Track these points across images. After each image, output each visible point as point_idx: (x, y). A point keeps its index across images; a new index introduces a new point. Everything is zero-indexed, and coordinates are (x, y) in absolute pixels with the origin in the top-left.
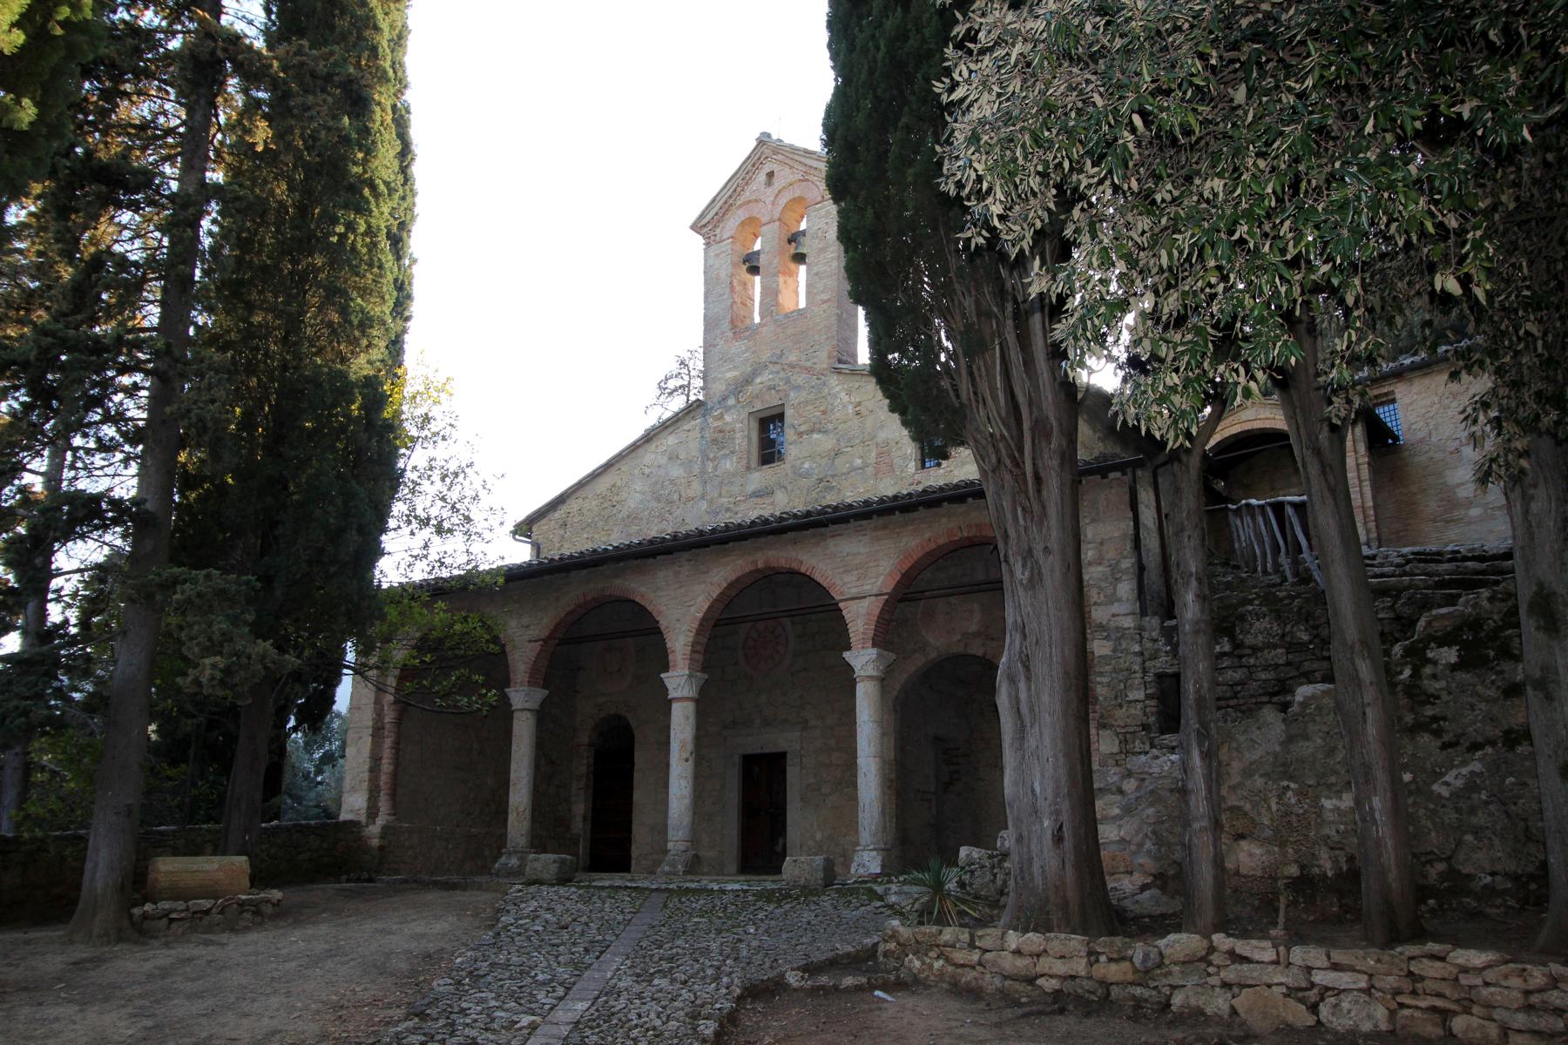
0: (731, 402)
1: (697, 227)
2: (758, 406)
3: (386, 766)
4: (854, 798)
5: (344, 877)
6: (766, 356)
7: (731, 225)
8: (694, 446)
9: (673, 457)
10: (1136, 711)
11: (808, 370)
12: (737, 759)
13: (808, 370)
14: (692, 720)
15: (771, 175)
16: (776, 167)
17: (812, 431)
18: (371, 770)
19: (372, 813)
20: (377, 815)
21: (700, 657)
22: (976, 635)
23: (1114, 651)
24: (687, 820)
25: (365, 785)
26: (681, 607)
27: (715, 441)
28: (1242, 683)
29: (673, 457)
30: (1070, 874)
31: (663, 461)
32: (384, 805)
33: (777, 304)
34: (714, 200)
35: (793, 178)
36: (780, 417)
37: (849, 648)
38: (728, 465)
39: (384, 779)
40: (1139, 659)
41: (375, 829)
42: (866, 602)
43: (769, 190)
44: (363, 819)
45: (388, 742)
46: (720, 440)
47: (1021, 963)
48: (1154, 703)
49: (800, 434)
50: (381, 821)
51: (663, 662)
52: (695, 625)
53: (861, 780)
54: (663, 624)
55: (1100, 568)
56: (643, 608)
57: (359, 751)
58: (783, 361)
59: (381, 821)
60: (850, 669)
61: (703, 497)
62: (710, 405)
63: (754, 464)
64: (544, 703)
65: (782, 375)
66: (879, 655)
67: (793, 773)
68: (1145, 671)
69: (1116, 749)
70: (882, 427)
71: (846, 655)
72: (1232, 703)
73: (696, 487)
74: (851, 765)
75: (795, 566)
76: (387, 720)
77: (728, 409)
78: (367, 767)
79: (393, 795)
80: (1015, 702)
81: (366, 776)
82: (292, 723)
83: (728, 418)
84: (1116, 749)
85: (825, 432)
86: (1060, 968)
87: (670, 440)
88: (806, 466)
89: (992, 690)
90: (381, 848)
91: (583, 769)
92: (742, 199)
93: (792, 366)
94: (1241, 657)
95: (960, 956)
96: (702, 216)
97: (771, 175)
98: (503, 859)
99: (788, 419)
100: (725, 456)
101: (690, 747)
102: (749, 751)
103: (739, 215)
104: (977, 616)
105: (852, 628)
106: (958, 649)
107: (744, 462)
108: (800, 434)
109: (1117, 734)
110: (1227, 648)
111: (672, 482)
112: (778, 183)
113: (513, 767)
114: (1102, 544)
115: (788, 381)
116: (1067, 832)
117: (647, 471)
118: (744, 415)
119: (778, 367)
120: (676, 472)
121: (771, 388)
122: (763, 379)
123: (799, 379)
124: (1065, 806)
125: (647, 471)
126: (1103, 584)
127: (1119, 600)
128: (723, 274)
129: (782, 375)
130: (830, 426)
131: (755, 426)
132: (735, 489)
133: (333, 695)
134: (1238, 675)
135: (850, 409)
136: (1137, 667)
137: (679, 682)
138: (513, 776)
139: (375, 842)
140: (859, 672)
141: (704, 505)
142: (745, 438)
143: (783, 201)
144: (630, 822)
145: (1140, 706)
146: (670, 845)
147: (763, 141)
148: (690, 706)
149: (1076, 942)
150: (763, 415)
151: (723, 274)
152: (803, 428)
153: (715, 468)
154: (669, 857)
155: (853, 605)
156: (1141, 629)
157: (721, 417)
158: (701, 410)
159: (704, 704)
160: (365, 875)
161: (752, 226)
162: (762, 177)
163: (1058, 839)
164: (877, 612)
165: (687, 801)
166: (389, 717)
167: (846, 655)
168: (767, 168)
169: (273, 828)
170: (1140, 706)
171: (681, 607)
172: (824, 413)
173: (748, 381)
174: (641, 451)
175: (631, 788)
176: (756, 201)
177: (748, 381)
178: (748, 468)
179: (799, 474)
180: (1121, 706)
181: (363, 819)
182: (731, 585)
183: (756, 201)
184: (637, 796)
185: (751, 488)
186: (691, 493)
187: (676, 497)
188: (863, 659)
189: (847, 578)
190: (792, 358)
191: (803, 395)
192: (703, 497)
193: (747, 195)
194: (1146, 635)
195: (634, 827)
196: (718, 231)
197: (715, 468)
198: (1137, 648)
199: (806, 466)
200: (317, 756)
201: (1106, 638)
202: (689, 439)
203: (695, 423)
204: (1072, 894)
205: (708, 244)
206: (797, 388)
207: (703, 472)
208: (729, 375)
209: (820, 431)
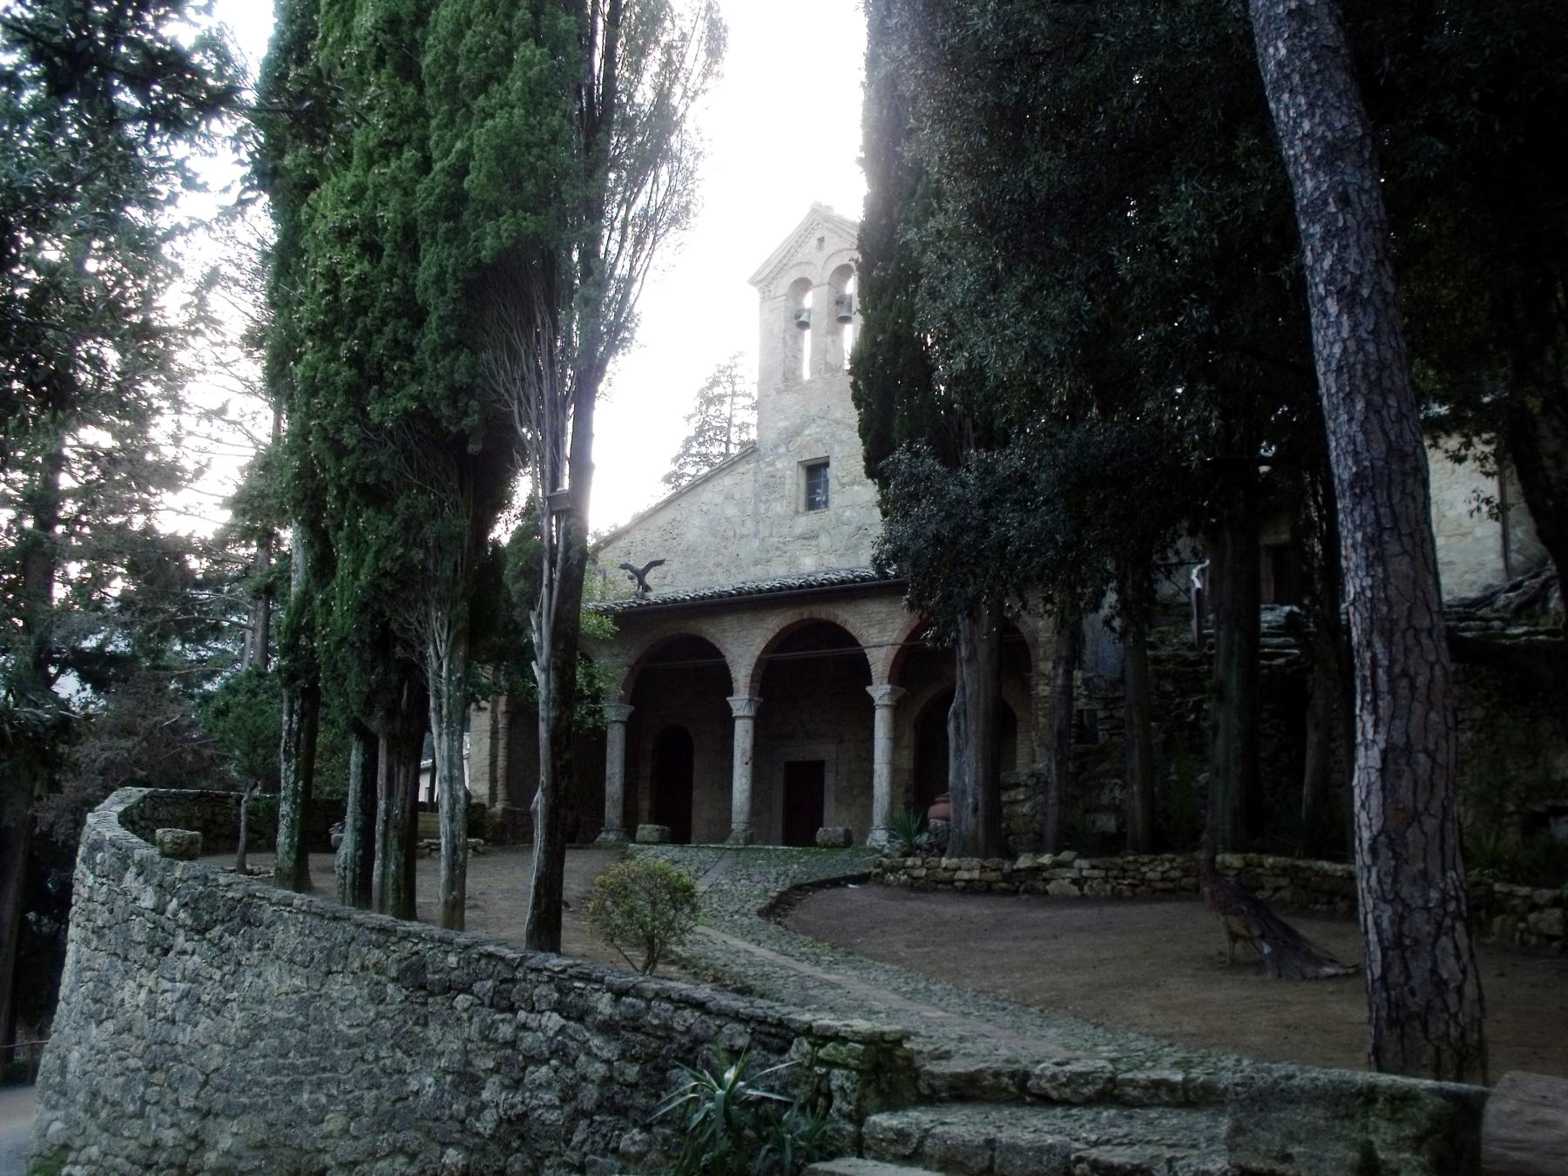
0: (782, 450)
1: (754, 282)
2: (806, 457)
4: (871, 796)
6: (814, 410)
8: (748, 488)
15: (821, 240)
16: (826, 234)
19: (493, 796)
21: (757, 686)
24: (746, 808)
26: (743, 650)
27: (766, 485)
29: (729, 497)
30: (981, 828)
31: (720, 499)
35: (841, 246)
36: (827, 465)
37: (870, 683)
38: (779, 508)
39: (500, 772)
42: (884, 650)
45: (502, 743)
46: (771, 485)
47: (947, 875)
49: (843, 485)
52: (754, 660)
53: (876, 780)
56: (713, 646)
59: (499, 806)
60: (871, 700)
61: (756, 535)
63: (801, 508)
64: (630, 717)
65: (828, 429)
66: (892, 690)
67: (830, 779)
71: (868, 689)
73: (750, 526)
74: (870, 773)
75: (832, 618)
77: (780, 456)
79: (508, 786)
80: (957, 729)
83: (779, 465)
86: (966, 876)
87: (727, 481)
88: (848, 514)
89: (945, 723)
91: (649, 771)
95: (916, 873)
97: (821, 240)
98: (603, 835)
100: (776, 499)
101: (749, 754)
103: (795, 275)
105: (873, 669)
107: (792, 507)
108: (843, 485)
111: (727, 519)
113: (608, 765)
115: (833, 436)
116: (980, 805)
118: (794, 463)
119: (825, 422)
120: (731, 510)
121: (817, 441)
122: (812, 431)
124: (980, 791)
129: (828, 429)
131: (802, 474)
132: (785, 531)
137: (740, 703)
138: (608, 772)
140: (877, 702)
141: (756, 543)
142: (794, 483)
146: (734, 826)
149: (975, 861)
152: (845, 480)
154: (733, 834)
157: (772, 464)
158: (755, 456)
159: (761, 722)
162: (814, 242)
163: (975, 810)
164: (892, 657)
165: (747, 794)
167: (868, 689)
168: (818, 234)
171: (743, 650)
173: (798, 432)
174: (700, 489)
178: (797, 512)
179: (841, 522)
182: (782, 631)
185: (798, 530)
186: (745, 531)
187: (731, 534)
188: (880, 691)
189: (871, 631)
192: (756, 535)
197: (767, 510)
199: (848, 514)
202: (742, 482)
203: (748, 467)
204: (981, 840)
205: (763, 299)
206: (841, 442)
207: (756, 513)
208: (781, 424)
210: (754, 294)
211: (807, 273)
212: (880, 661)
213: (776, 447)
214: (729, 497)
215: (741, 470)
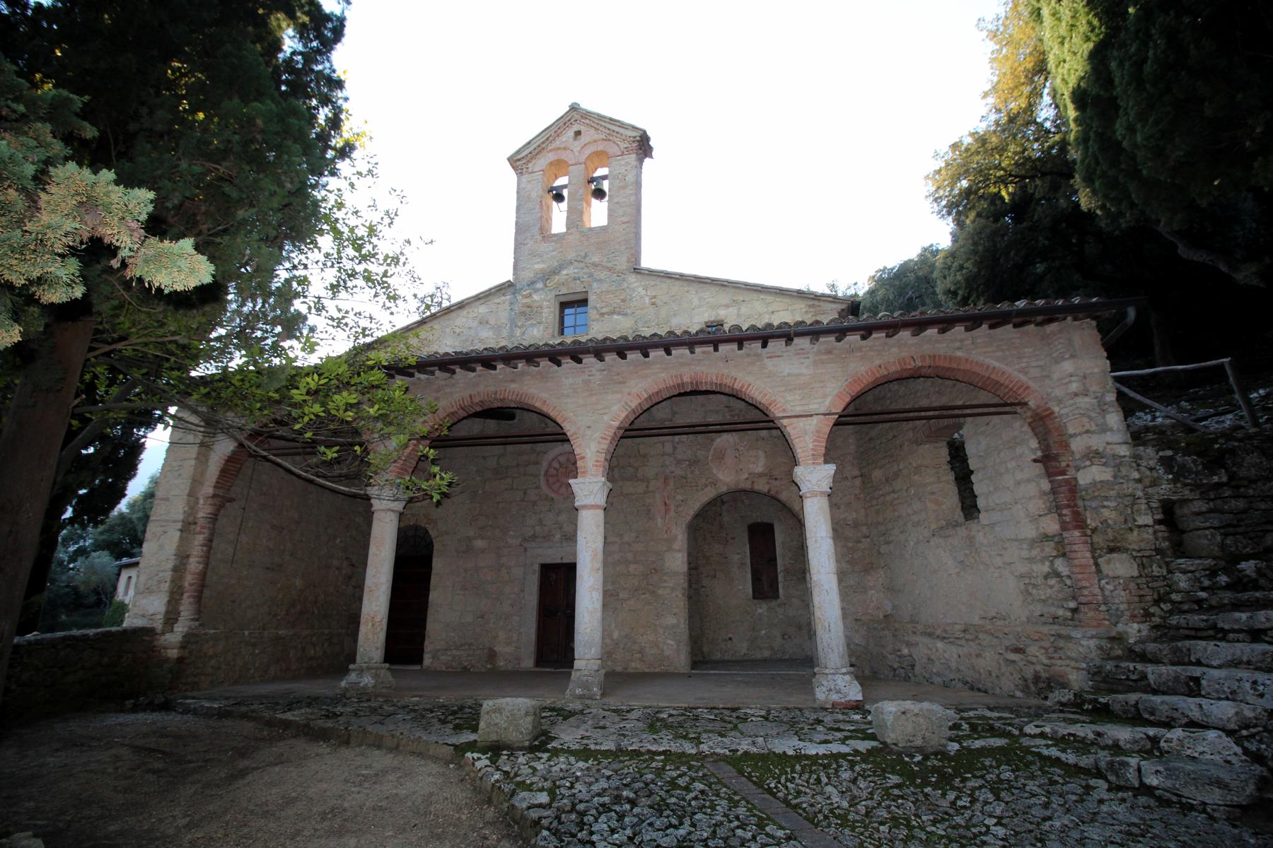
0: (539, 285)
2: (564, 291)
3: (194, 565)
5: (129, 703)
7: (542, 162)
9: (483, 322)
10: (1148, 535)
11: (610, 269)
12: (537, 567)
13: (610, 269)
14: (602, 529)
15: (578, 133)
16: (582, 128)
17: (613, 313)
18: (175, 569)
19: (171, 618)
20: (176, 620)
22: (760, 475)
23: (1115, 477)
24: (597, 636)
25: (166, 586)
26: (592, 412)
27: (523, 313)
28: (1244, 512)
31: (475, 324)
32: (186, 609)
33: (582, 220)
34: (529, 143)
35: (596, 137)
36: (583, 302)
39: (189, 580)
40: (1140, 486)
41: (172, 640)
42: (815, 420)
43: (577, 143)
44: (158, 625)
45: (200, 539)
48: (1162, 528)
50: (181, 628)
51: (571, 467)
54: (569, 429)
55: (1087, 399)
57: (161, 547)
58: (587, 260)
59: (181, 628)
62: (518, 286)
68: (1148, 498)
69: (1136, 573)
70: (675, 315)
72: (1240, 530)
76: (201, 514)
77: (536, 291)
78: (170, 565)
79: (199, 598)
81: (168, 575)
82: (69, 513)
83: (536, 297)
84: (1136, 573)
85: (625, 315)
87: (482, 309)
90: (180, 660)
92: (553, 146)
93: (595, 265)
94: (1238, 487)
96: (518, 152)
97: (578, 133)
98: (353, 677)
99: (590, 303)
100: (532, 325)
102: (548, 561)
103: (551, 157)
104: (762, 461)
106: (748, 486)
108: (603, 315)
109: (1135, 558)
110: (1225, 479)
112: (584, 139)
113: (370, 572)
114: (1085, 377)
115: (591, 275)
117: (458, 330)
118: (551, 296)
119: (582, 265)
121: (575, 279)
123: (603, 275)
125: (458, 330)
126: (1093, 414)
127: (1111, 430)
128: (534, 195)
129: (586, 270)
130: (629, 311)
133: (125, 489)
134: (1241, 504)
135: (647, 300)
136: (1139, 493)
139: (174, 653)
143: (588, 151)
144: (425, 620)
145: (1151, 530)
147: (574, 108)
148: (600, 514)
150: (564, 299)
151: (534, 195)
152: (604, 310)
153: (524, 333)
155: (801, 423)
156: (1137, 458)
158: (512, 290)
160: (160, 699)
161: (559, 166)
162: (571, 133)
166: (204, 511)
168: (576, 128)
169: (29, 643)
170: (1151, 530)
172: (623, 301)
173: (555, 272)
174: (453, 315)
175: (428, 590)
176: (565, 149)
177: (555, 272)
180: (1131, 529)
181: (158, 625)
183: (565, 149)
184: (433, 596)
190: (595, 259)
191: (605, 287)
193: (557, 143)
194: (1144, 463)
195: (429, 619)
196: (530, 165)
198: (1136, 475)
200: (72, 549)
201: (1104, 465)
209: (619, 314)
210: (510, 177)
211: (564, 156)
212: (807, 435)
213: (533, 283)
214: (483, 322)
215: (497, 301)
